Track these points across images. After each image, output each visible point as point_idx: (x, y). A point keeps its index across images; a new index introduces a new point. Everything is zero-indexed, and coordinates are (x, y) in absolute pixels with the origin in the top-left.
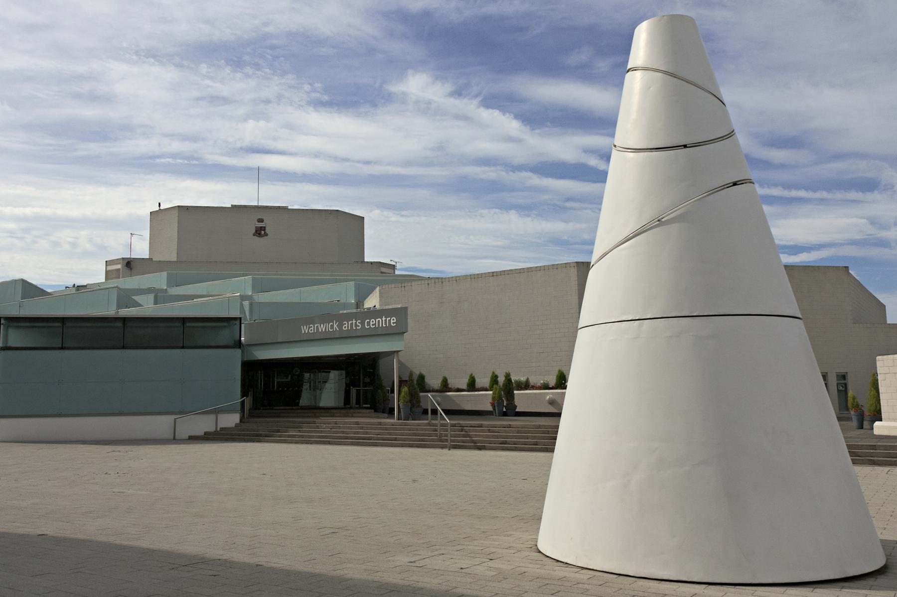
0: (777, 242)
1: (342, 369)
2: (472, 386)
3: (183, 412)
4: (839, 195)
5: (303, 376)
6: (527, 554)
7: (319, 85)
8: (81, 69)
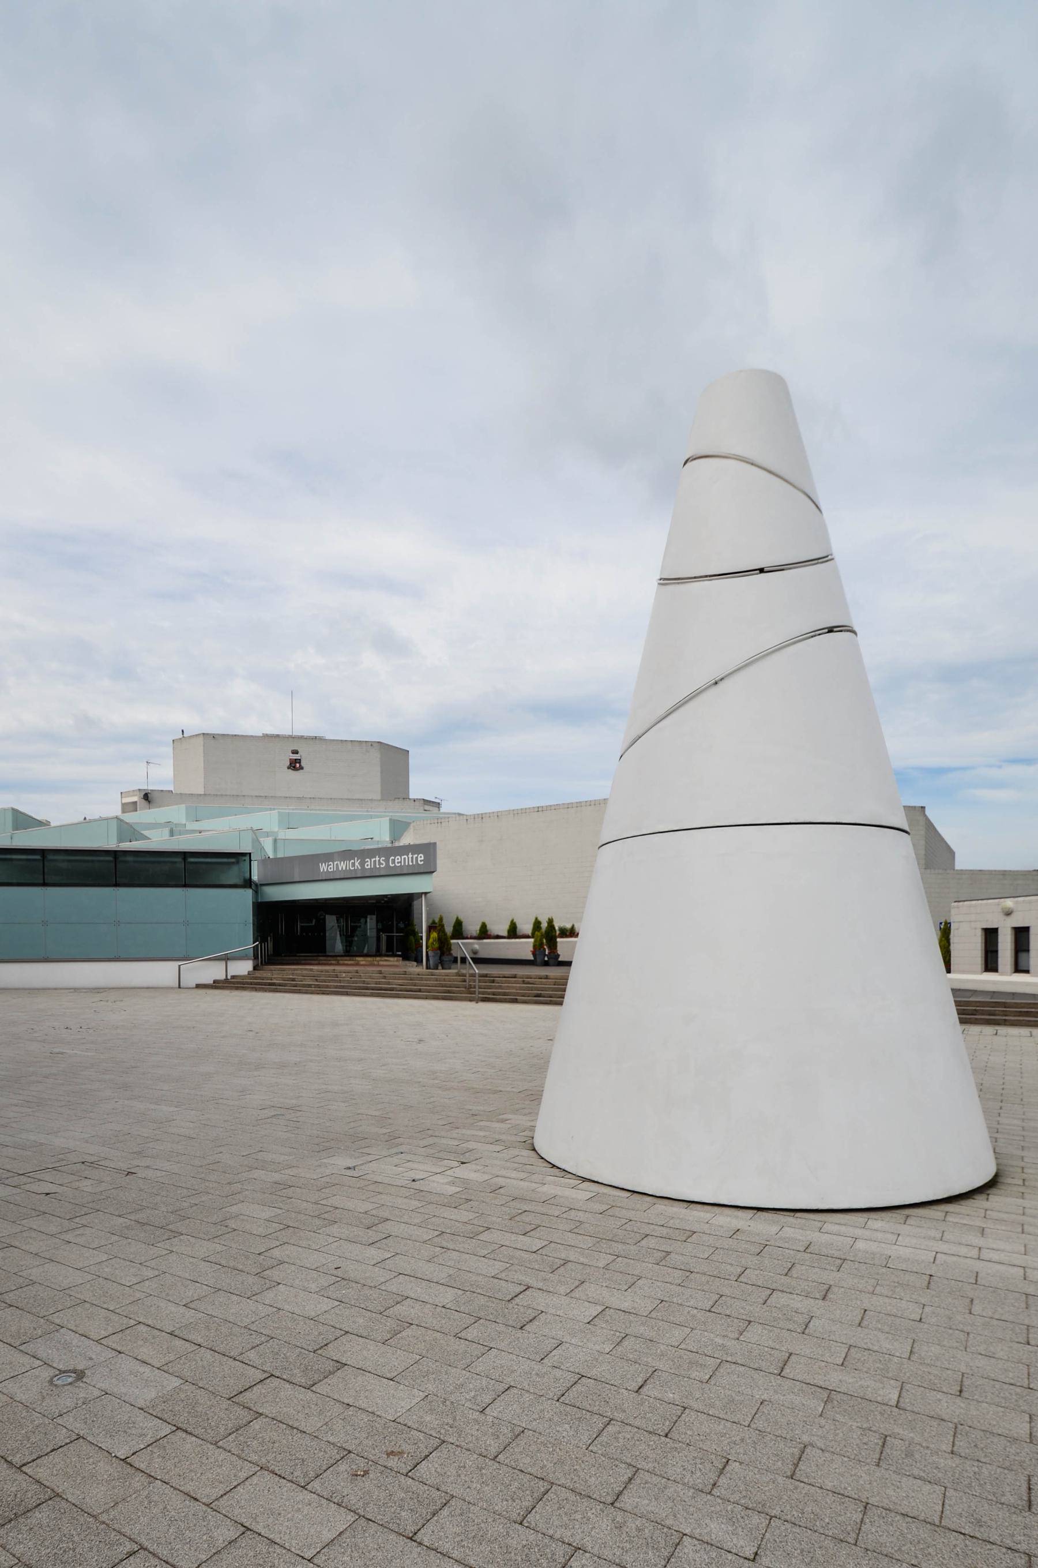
2: (513, 932)
3: (187, 958)
6: (516, 1152)
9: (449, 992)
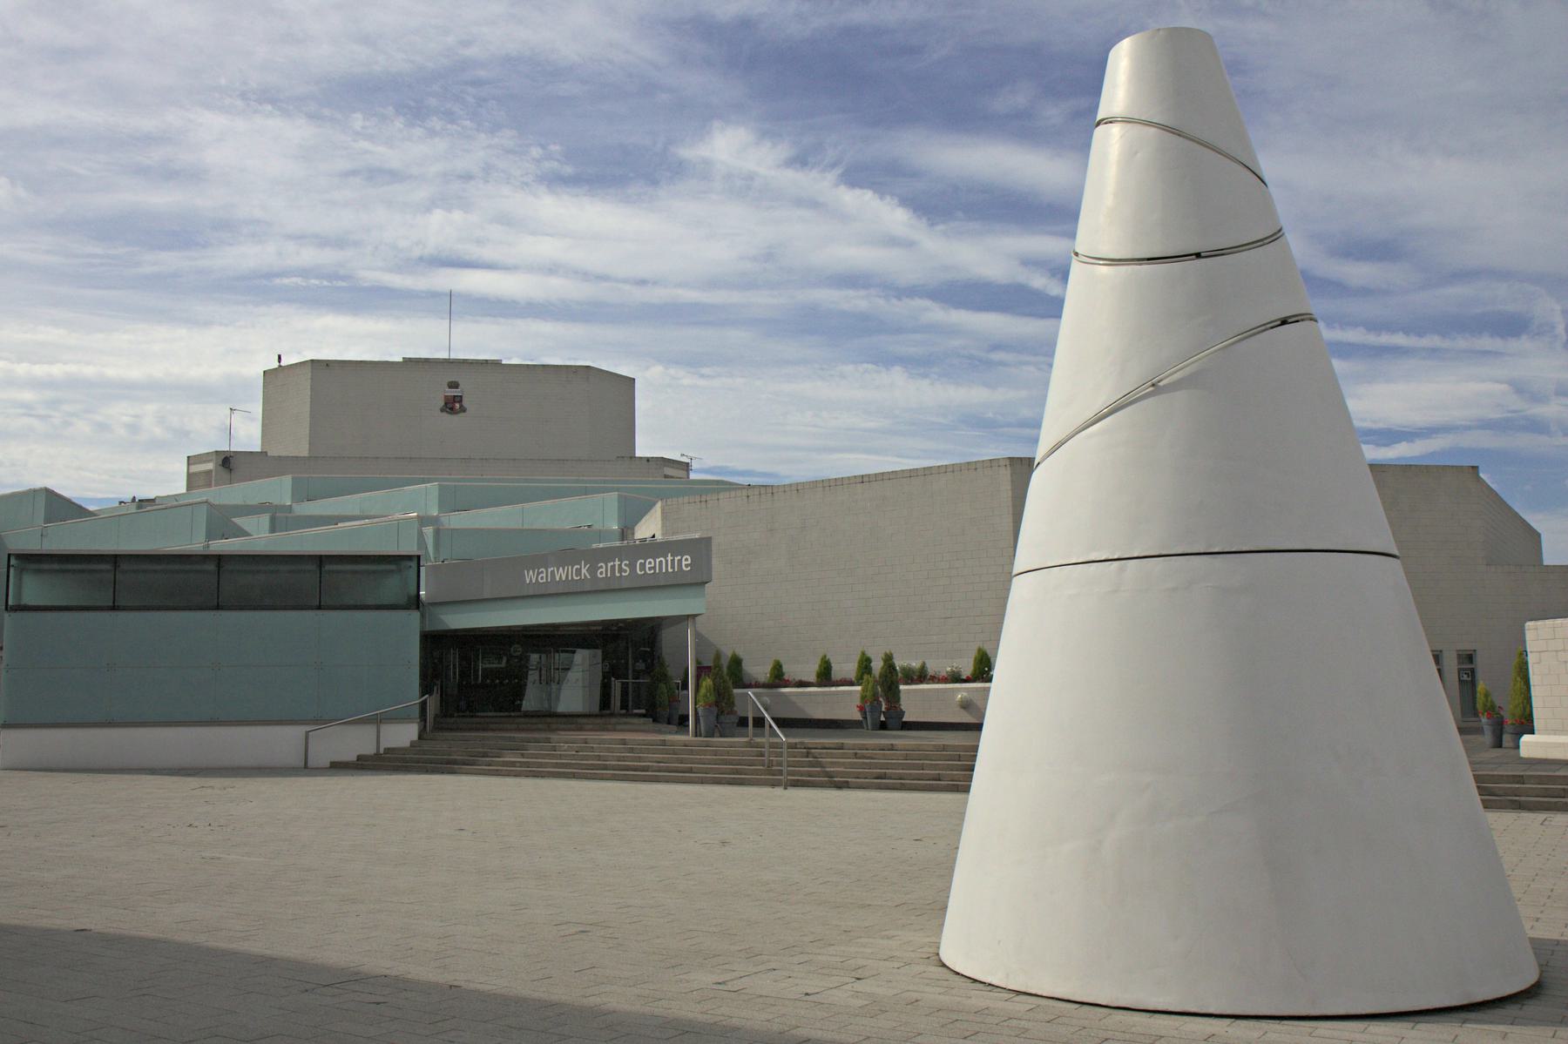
0: (1356, 423)
1: (596, 647)
2: (825, 676)
4: (1462, 343)
5: (528, 659)
6: (921, 968)
7: (558, 148)
8: (147, 124)
9: (738, 772)
